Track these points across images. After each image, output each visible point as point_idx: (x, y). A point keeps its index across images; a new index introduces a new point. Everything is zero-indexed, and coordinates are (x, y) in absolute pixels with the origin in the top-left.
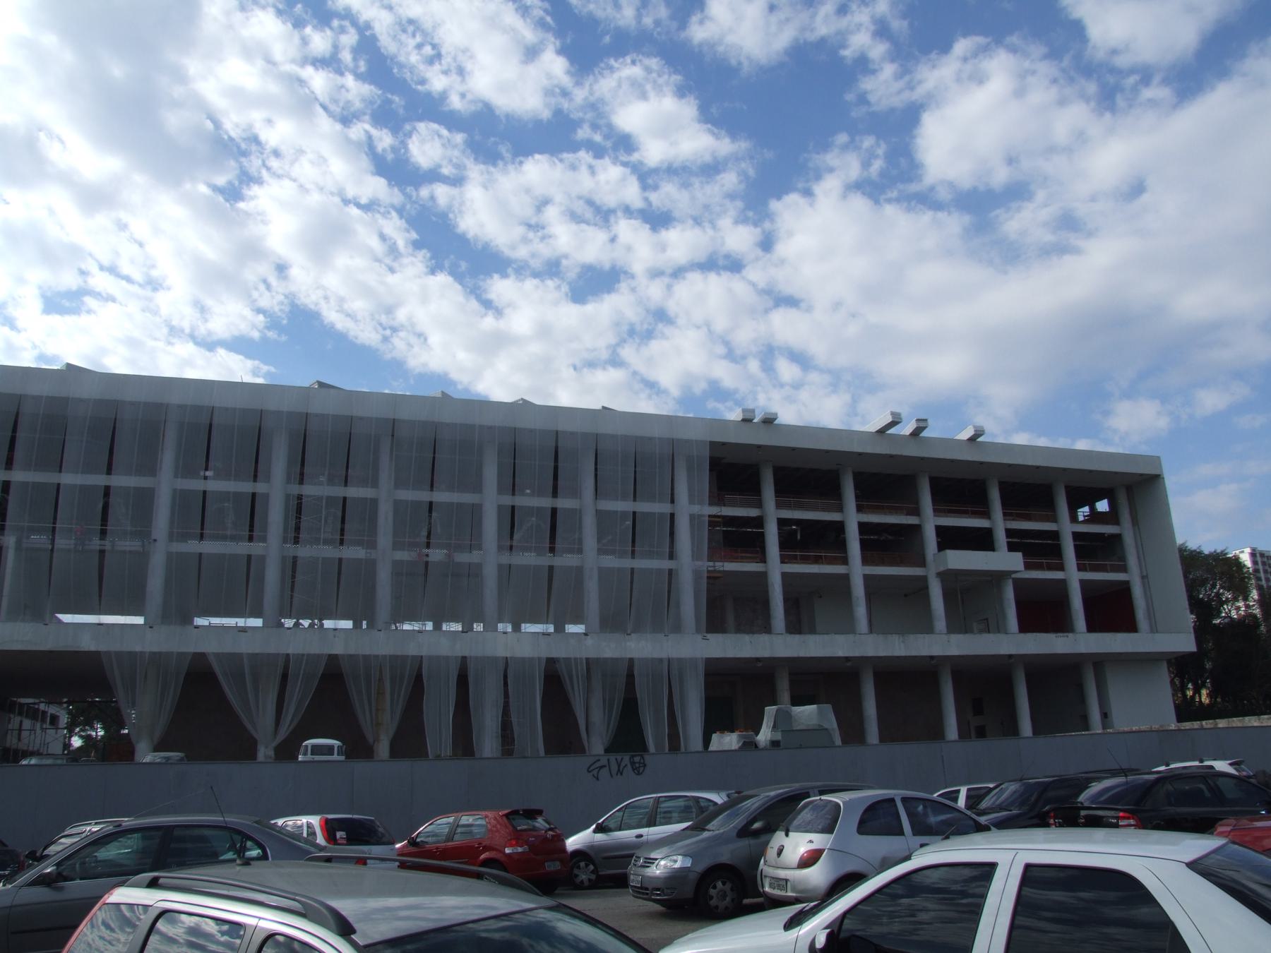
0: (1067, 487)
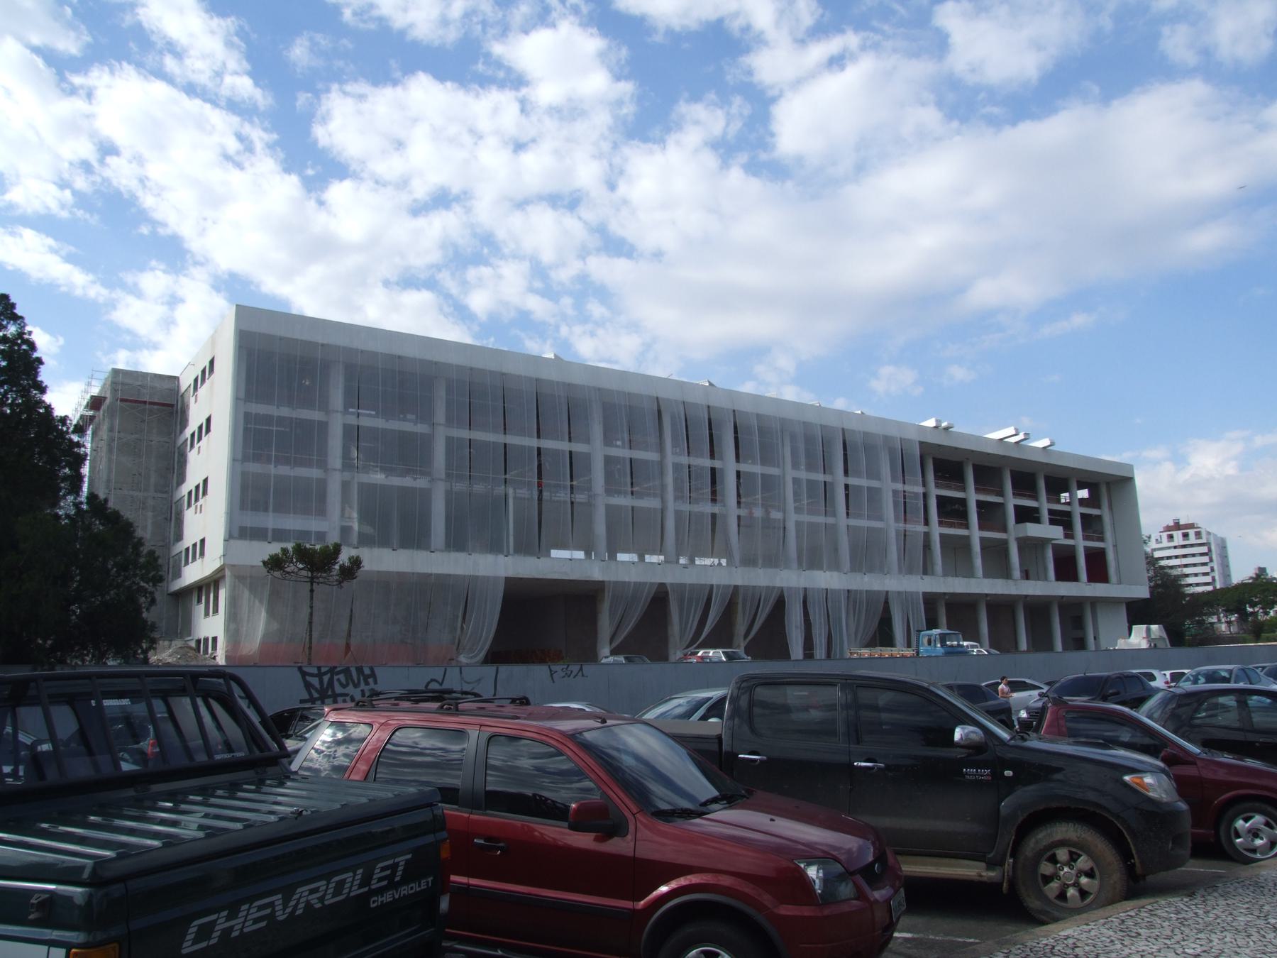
0: (935, 460)
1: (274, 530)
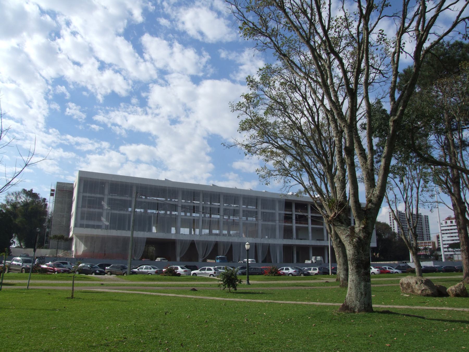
1: (86, 225)
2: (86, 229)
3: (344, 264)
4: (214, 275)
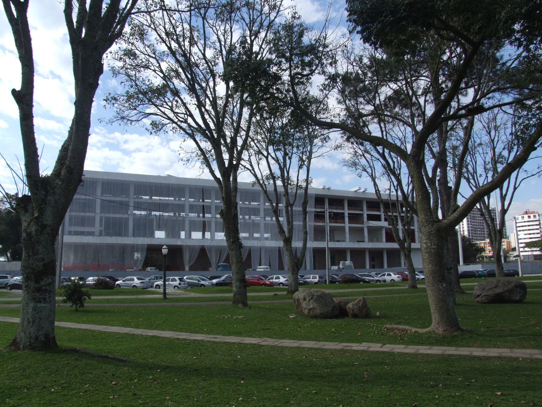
1: (74, 231)
2: (74, 237)
3: (237, 273)
4: (179, 286)
